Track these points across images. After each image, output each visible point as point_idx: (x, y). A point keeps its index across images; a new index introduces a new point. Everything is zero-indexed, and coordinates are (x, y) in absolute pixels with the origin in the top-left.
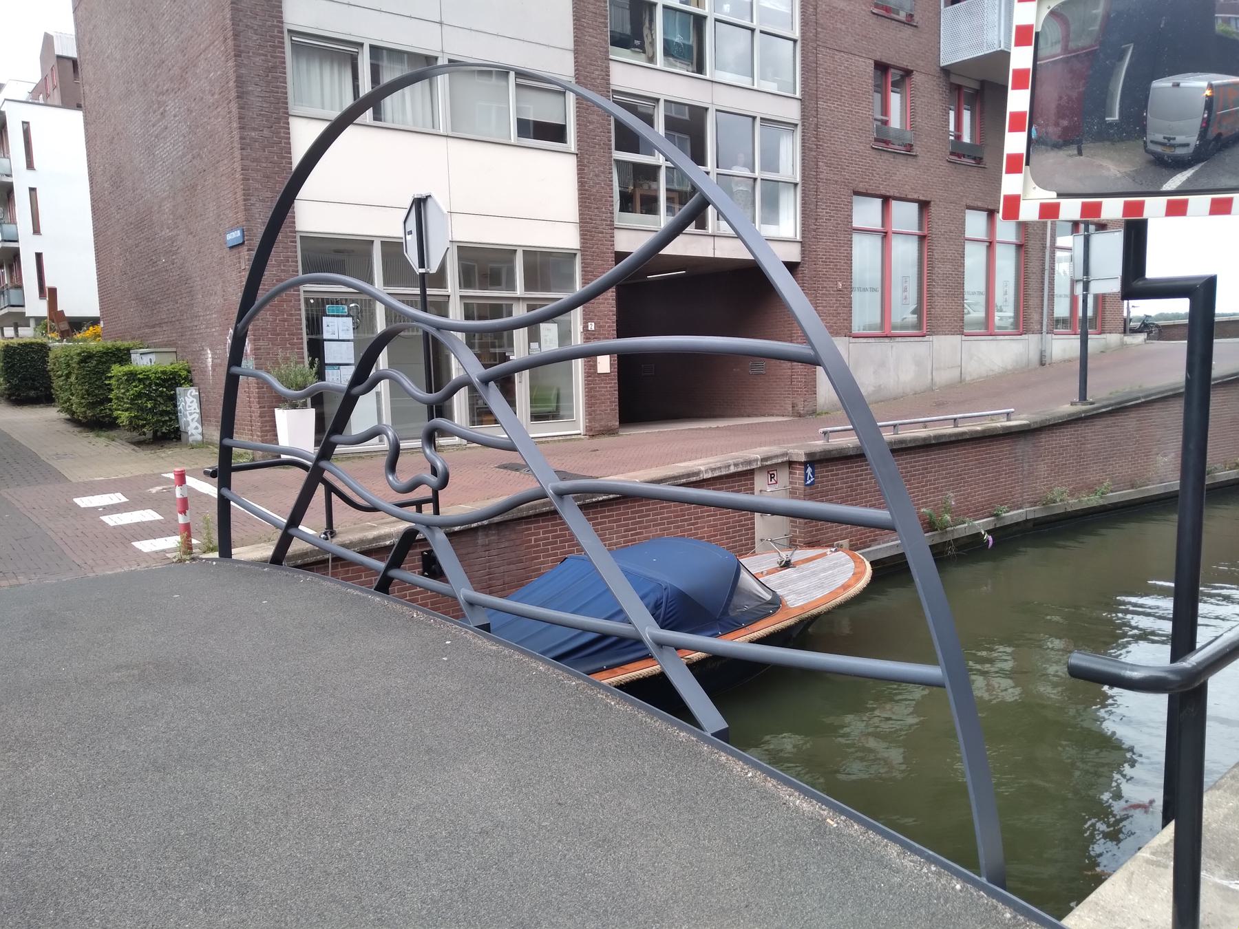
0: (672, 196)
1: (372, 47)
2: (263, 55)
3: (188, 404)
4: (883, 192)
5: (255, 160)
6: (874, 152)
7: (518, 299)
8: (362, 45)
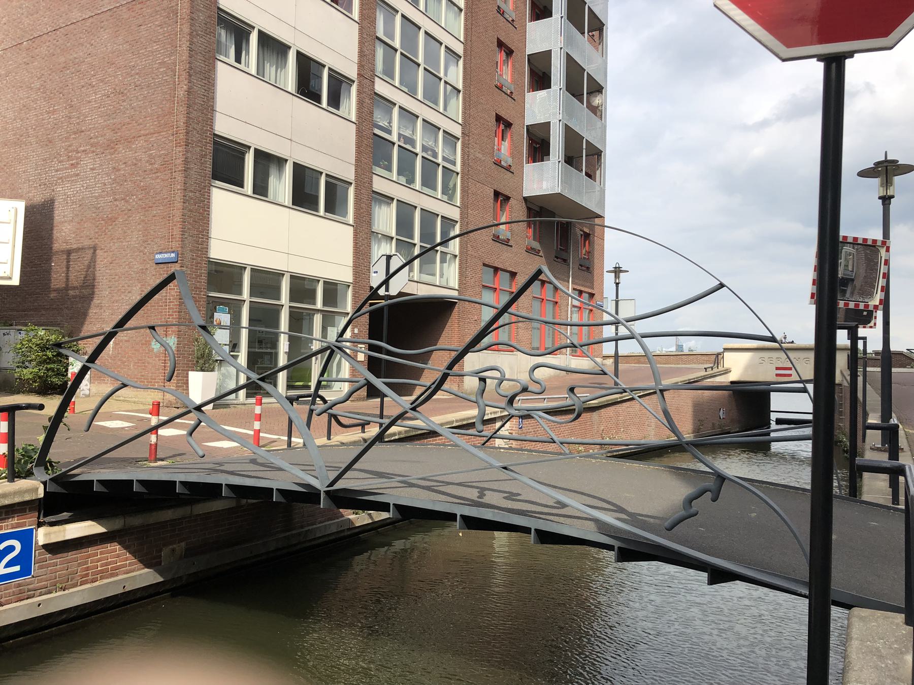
1: (256, 150)
4: (496, 265)
5: (190, 211)
6: (493, 242)
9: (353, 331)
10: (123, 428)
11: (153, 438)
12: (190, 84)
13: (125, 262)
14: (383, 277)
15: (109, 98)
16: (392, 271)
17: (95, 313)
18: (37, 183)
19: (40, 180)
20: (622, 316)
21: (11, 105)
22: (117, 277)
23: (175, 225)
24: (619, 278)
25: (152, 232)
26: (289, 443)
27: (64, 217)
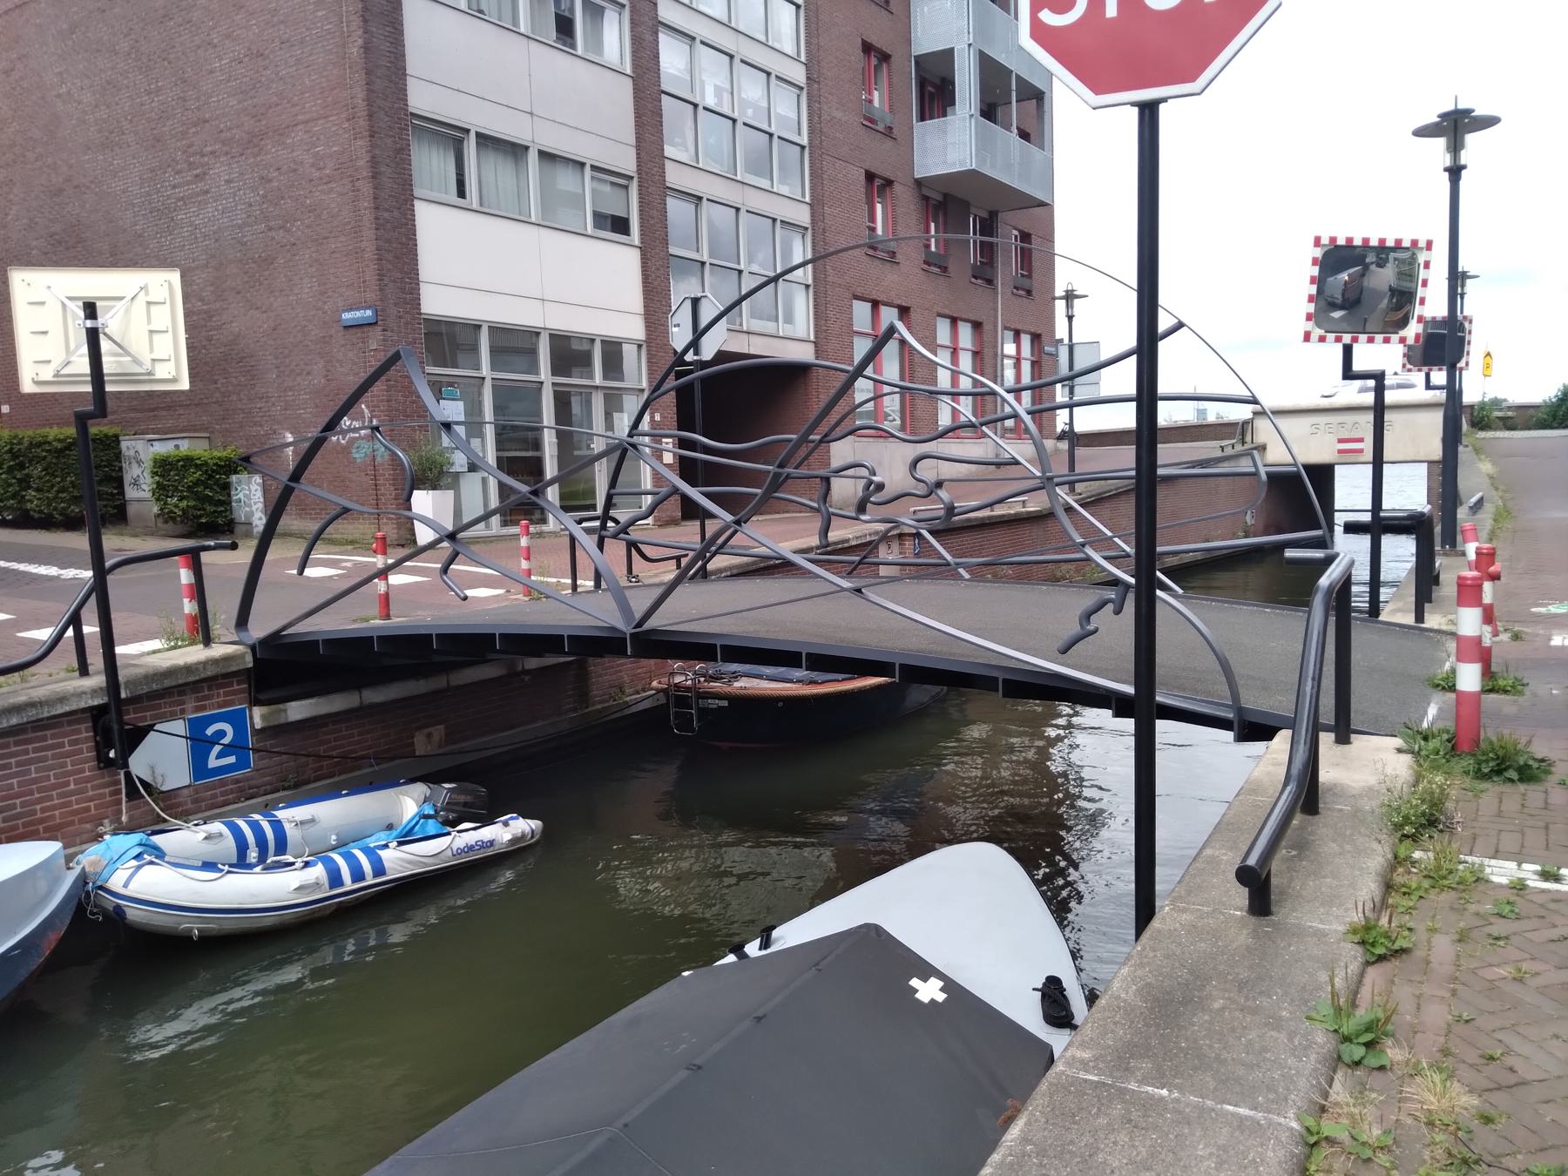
1: (478, 135)
2: (391, 136)
3: (253, 492)
4: (875, 297)
5: (388, 241)
7: (597, 387)
8: (467, 131)
9: (652, 418)
10: (331, 577)
11: (380, 586)
12: (366, 36)
13: (296, 326)
14: (689, 337)
15: (242, 65)
16: (704, 322)
17: (260, 408)
18: (146, 209)
19: (150, 204)
20: (1078, 367)
21: (86, 81)
22: (286, 351)
23: (367, 266)
24: (1072, 308)
25: (332, 278)
26: (575, 587)
27: (194, 261)
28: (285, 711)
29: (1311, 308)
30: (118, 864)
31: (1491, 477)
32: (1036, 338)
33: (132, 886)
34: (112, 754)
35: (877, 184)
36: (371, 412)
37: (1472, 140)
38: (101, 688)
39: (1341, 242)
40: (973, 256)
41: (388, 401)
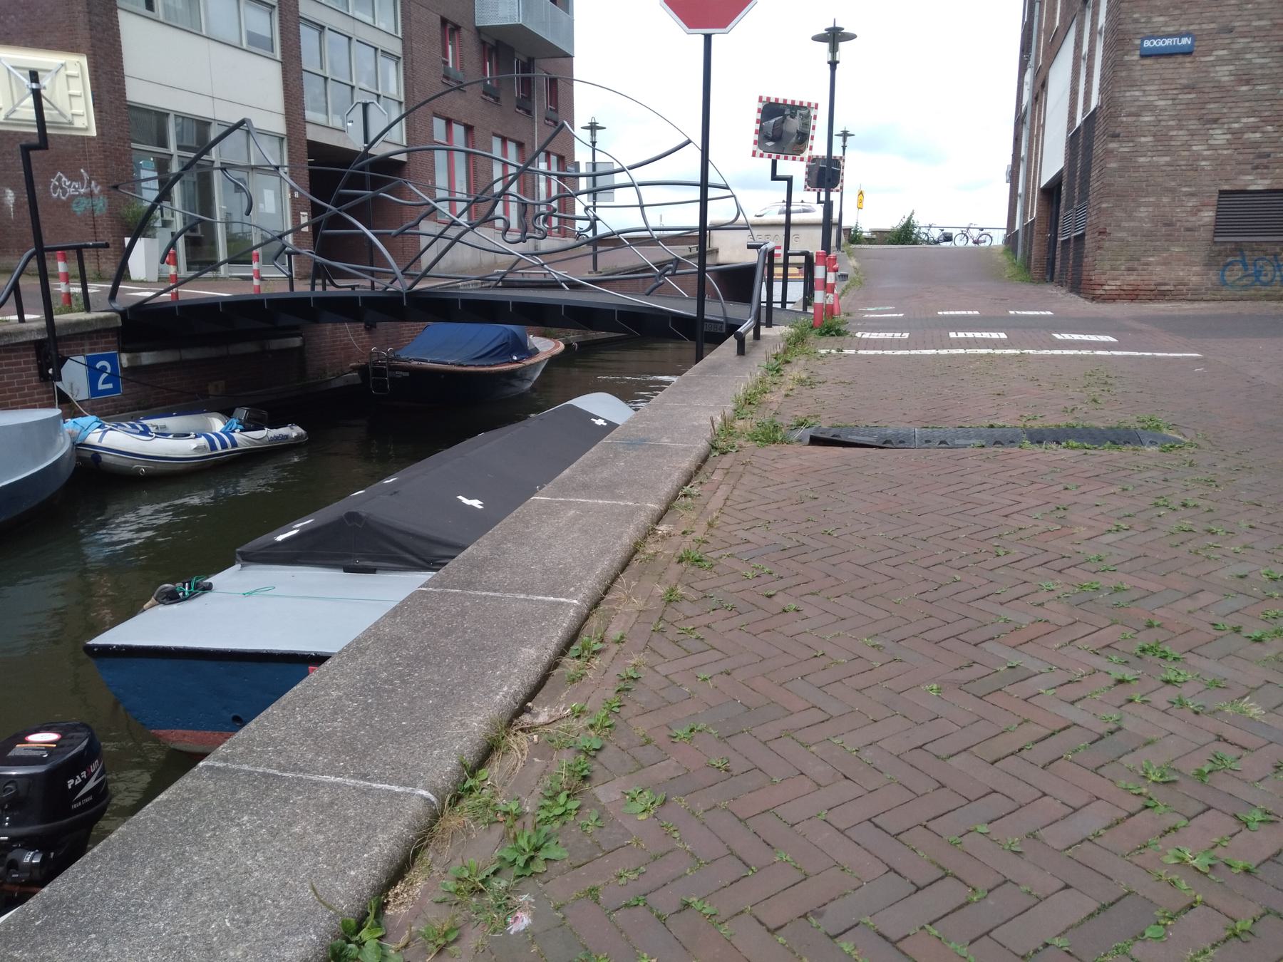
0: (63, 62)
4: (449, 116)
5: (100, 41)
24: (595, 135)
28: (140, 357)
29: (757, 137)
30: (89, 431)
31: (855, 268)
32: (561, 159)
33: (103, 441)
34: (50, 371)
35: (449, 28)
36: (90, 175)
37: (843, 46)
38: (42, 329)
39: (773, 100)
40: (517, 92)
41: (105, 167)
